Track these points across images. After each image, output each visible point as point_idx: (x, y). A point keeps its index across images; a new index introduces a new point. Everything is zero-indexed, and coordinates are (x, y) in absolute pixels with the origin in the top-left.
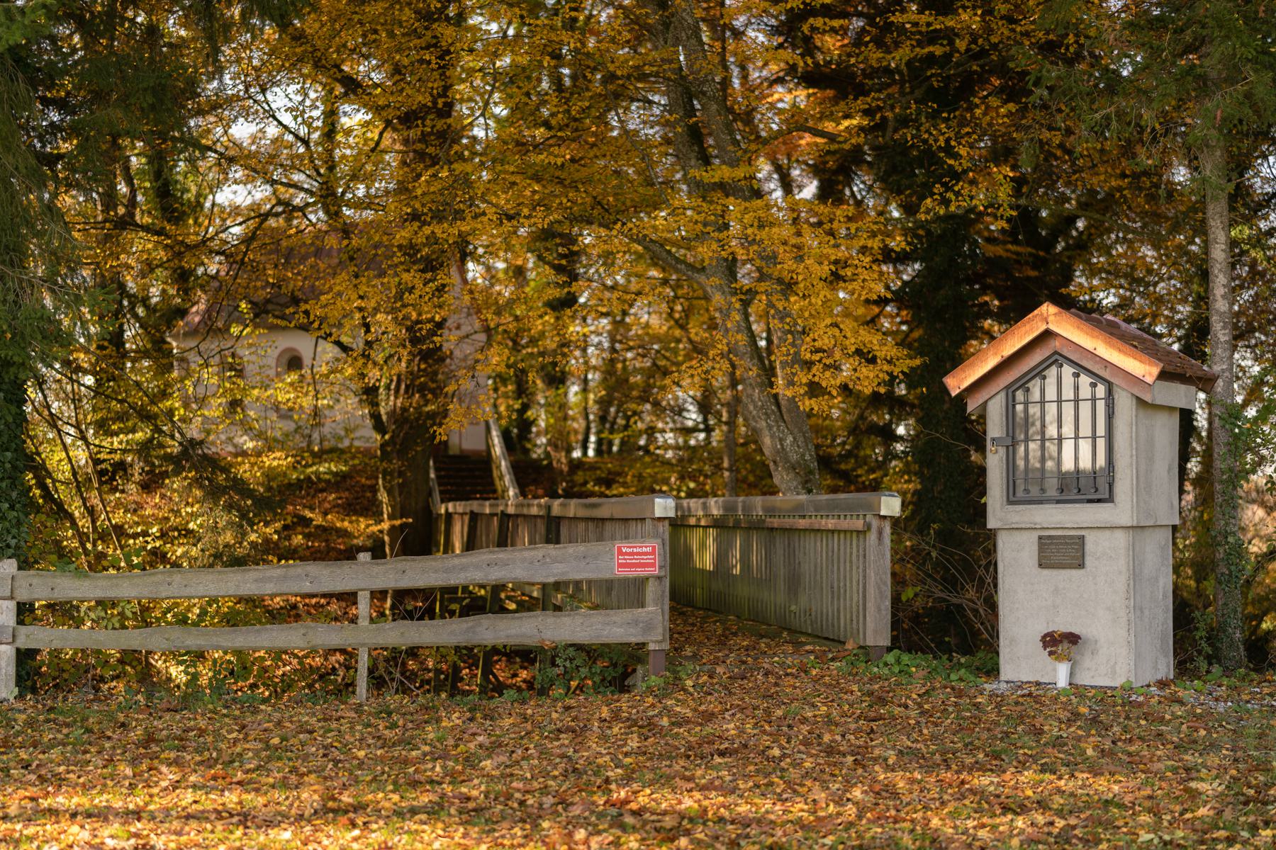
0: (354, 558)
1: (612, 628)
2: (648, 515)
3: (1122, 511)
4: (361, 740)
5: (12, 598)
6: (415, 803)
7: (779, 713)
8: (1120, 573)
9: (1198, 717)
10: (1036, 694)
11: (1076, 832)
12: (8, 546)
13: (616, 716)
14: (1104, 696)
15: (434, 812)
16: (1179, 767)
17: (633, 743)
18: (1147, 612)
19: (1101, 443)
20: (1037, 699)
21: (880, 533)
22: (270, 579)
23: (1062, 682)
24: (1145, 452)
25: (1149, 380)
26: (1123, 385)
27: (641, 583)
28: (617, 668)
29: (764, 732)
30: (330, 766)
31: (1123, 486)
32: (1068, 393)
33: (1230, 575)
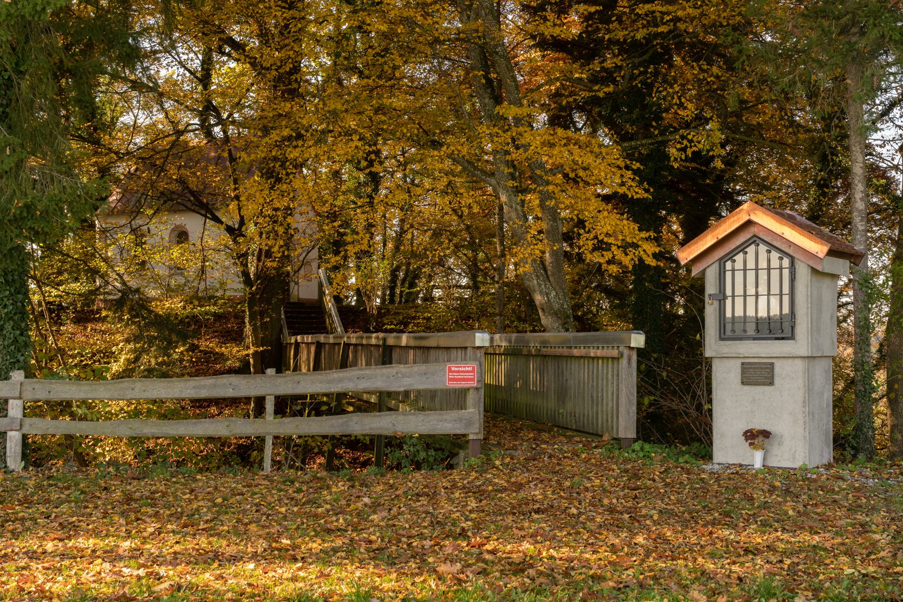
0: (264, 373)
1: (443, 423)
2: (468, 345)
3: (801, 345)
4: (279, 500)
5: (20, 398)
6: (333, 544)
7: (568, 483)
8: (799, 388)
9: (858, 490)
10: (740, 472)
11: (800, 567)
12: (18, 361)
13: (454, 486)
14: (789, 474)
15: (350, 551)
16: (855, 524)
17: (473, 504)
18: (816, 416)
19: (786, 299)
20: (742, 476)
21: (630, 359)
22: (204, 387)
23: (758, 464)
24: (816, 305)
25: (821, 255)
26: (802, 259)
27: (464, 392)
28: (443, 451)
29: (561, 497)
30: (264, 518)
31: (802, 328)
32: (763, 264)
33: (865, 391)
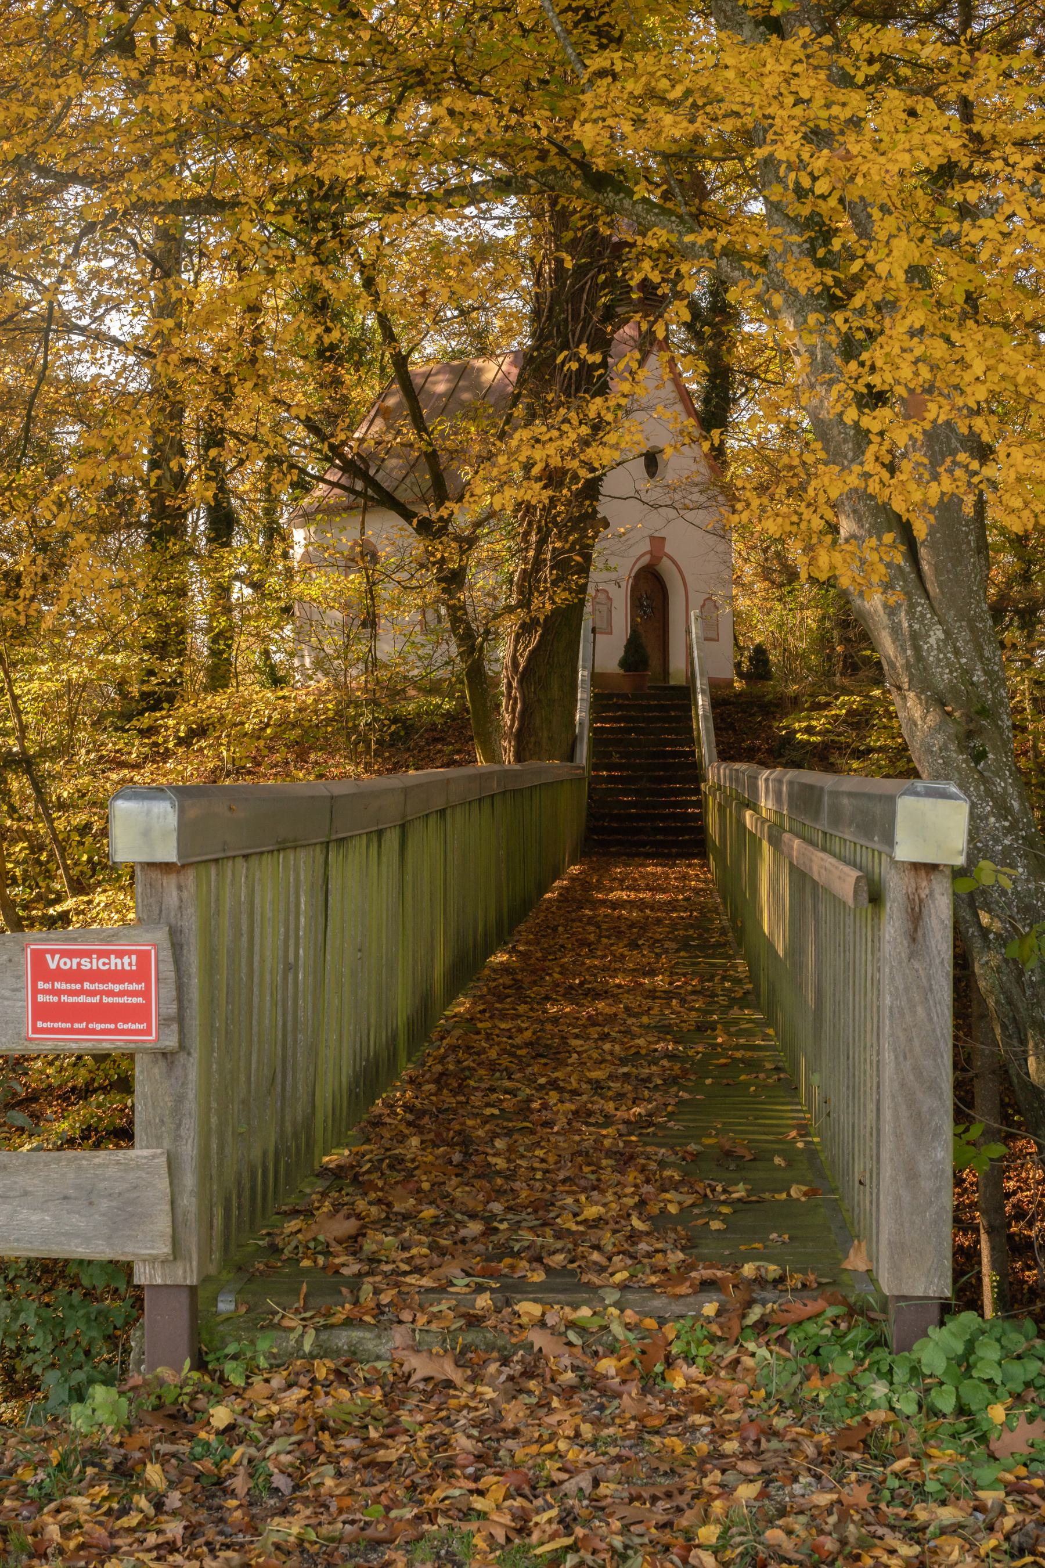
21: (916, 915)
